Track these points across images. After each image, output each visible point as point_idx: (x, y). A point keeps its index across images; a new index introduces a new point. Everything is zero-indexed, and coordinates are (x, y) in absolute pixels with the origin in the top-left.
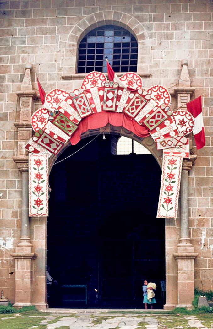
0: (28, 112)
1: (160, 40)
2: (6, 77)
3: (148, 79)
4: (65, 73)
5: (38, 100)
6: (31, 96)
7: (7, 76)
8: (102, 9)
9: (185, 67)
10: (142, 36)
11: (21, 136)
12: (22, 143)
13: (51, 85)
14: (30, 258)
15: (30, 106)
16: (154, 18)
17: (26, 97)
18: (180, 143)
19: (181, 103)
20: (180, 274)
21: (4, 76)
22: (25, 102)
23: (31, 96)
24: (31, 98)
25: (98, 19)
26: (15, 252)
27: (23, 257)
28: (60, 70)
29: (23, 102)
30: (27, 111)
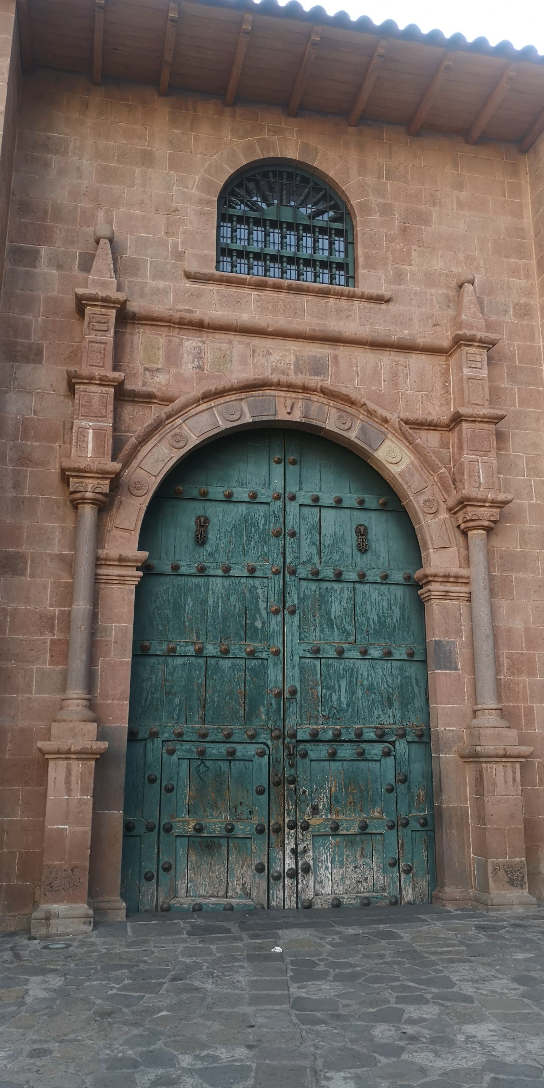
0: (103, 346)
1: (404, 223)
2: (43, 253)
3: (384, 306)
4: (194, 267)
5: (127, 323)
6: (116, 305)
7: (44, 251)
8: (275, 132)
9: (468, 287)
10: (365, 207)
11: (83, 406)
12: (85, 423)
13: (158, 289)
14: (92, 756)
15: (112, 331)
16: (388, 172)
17: (102, 306)
18: (227, 764)
19: (470, 369)
20: (490, 804)
21: (37, 252)
22: (98, 320)
23: (116, 305)
24: (114, 311)
25: (265, 153)
26: (49, 740)
27: (75, 753)
28: (179, 256)
29: (93, 318)
30: (103, 343)
